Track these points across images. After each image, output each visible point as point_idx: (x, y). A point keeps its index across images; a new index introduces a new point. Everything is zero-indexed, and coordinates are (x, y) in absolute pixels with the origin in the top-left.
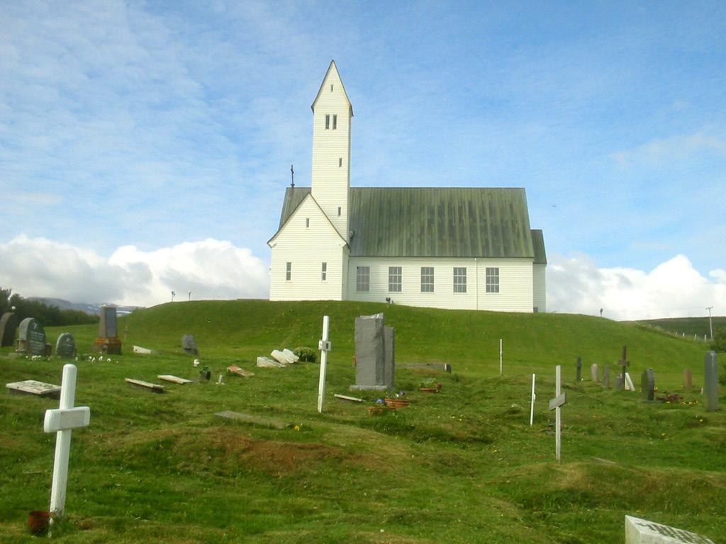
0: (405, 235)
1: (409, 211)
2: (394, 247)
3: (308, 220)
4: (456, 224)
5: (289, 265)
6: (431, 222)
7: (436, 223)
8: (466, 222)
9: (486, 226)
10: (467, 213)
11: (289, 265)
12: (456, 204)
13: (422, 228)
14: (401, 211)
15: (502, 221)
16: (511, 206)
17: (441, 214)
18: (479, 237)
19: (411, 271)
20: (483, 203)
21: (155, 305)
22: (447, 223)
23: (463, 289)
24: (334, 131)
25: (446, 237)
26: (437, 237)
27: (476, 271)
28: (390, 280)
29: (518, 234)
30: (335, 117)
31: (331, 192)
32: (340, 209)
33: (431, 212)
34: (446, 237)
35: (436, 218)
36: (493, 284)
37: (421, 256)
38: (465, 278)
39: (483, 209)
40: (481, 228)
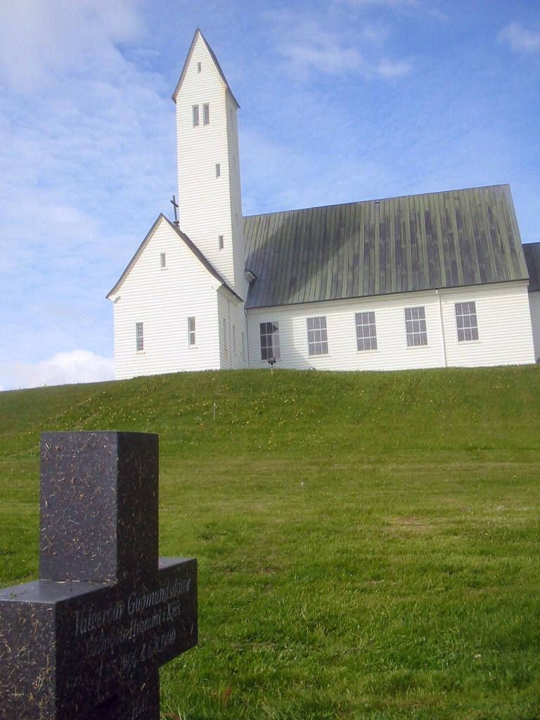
0: (330, 268)
1: (338, 233)
2: (312, 288)
3: (163, 256)
4: (408, 246)
5: (140, 327)
6: (368, 247)
7: (377, 248)
8: (422, 239)
9: (453, 242)
10: (423, 227)
11: (140, 327)
12: (407, 219)
13: (356, 258)
14: (326, 237)
15: (476, 234)
16: (490, 211)
17: (384, 232)
18: (442, 258)
19: (341, 322)
20: (446, 211)
21: (108, 380)
22: (392, 246)
23: (474, 335)
24: (207, 127)
25: (392, 265)
26: (378, 266)
27: (440, 312)
28: (310, 337)
29: (503, 251)
30: (206, 107)
31: (210, 214)
32: (221, 238)
33: (370, 234)
34: (392, 265)
35: (377, 241)
36: (467, 328)
37: (353, 297)
38: (423, 323)
39: (447, 221)
40: (445, 246)
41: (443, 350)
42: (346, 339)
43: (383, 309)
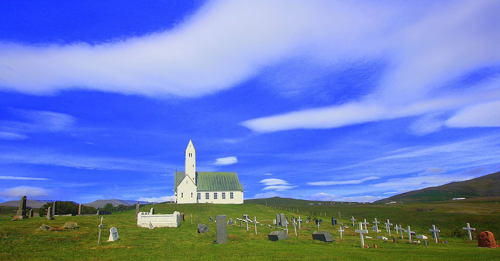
4: (221, 181)
22: (219, 181)
25: (219, 185)
35: (216, 180)
41: (228, 201)
42: (169, 188)
43: (122, 160)
